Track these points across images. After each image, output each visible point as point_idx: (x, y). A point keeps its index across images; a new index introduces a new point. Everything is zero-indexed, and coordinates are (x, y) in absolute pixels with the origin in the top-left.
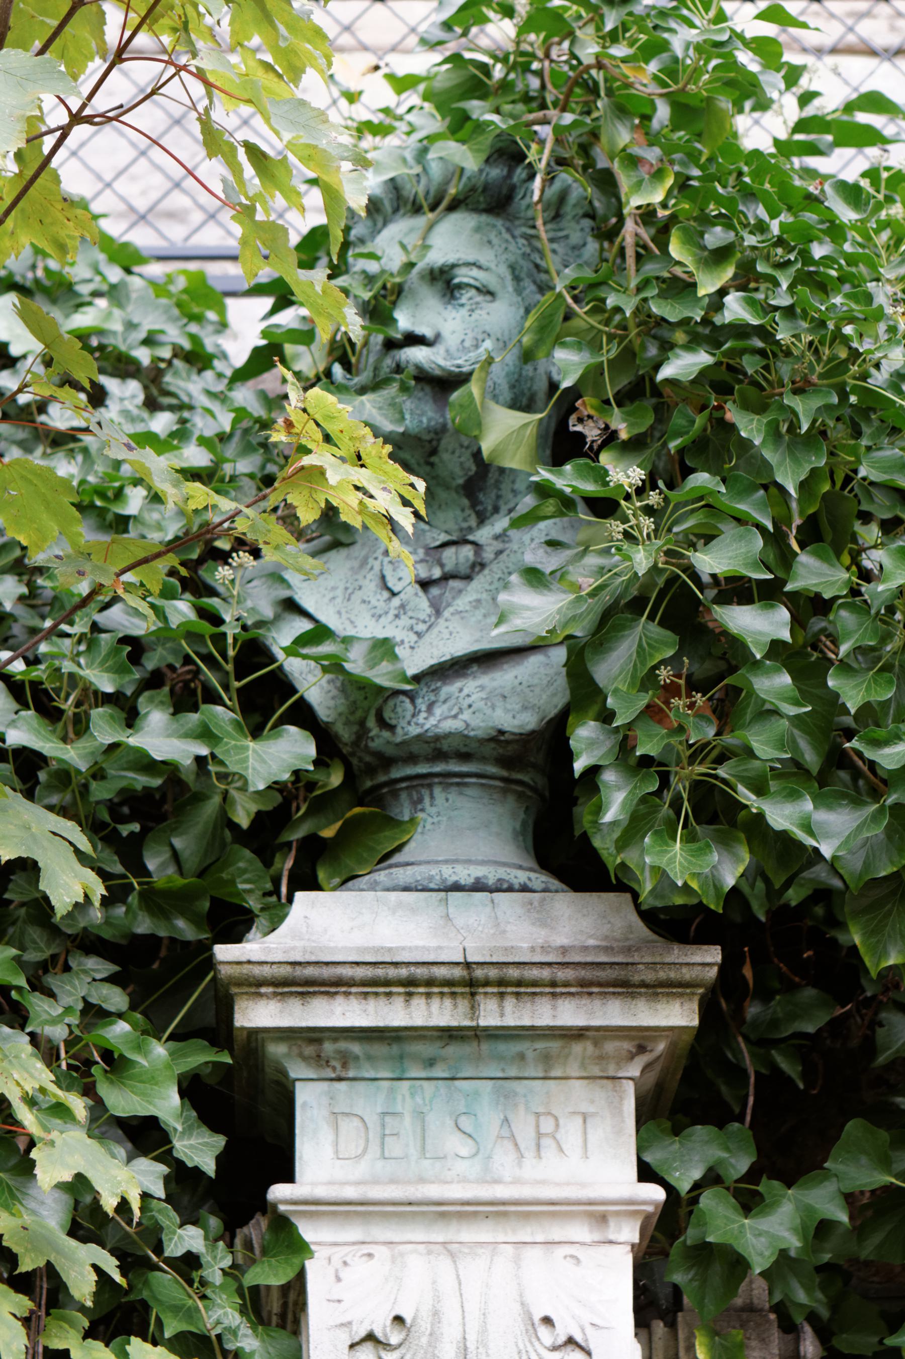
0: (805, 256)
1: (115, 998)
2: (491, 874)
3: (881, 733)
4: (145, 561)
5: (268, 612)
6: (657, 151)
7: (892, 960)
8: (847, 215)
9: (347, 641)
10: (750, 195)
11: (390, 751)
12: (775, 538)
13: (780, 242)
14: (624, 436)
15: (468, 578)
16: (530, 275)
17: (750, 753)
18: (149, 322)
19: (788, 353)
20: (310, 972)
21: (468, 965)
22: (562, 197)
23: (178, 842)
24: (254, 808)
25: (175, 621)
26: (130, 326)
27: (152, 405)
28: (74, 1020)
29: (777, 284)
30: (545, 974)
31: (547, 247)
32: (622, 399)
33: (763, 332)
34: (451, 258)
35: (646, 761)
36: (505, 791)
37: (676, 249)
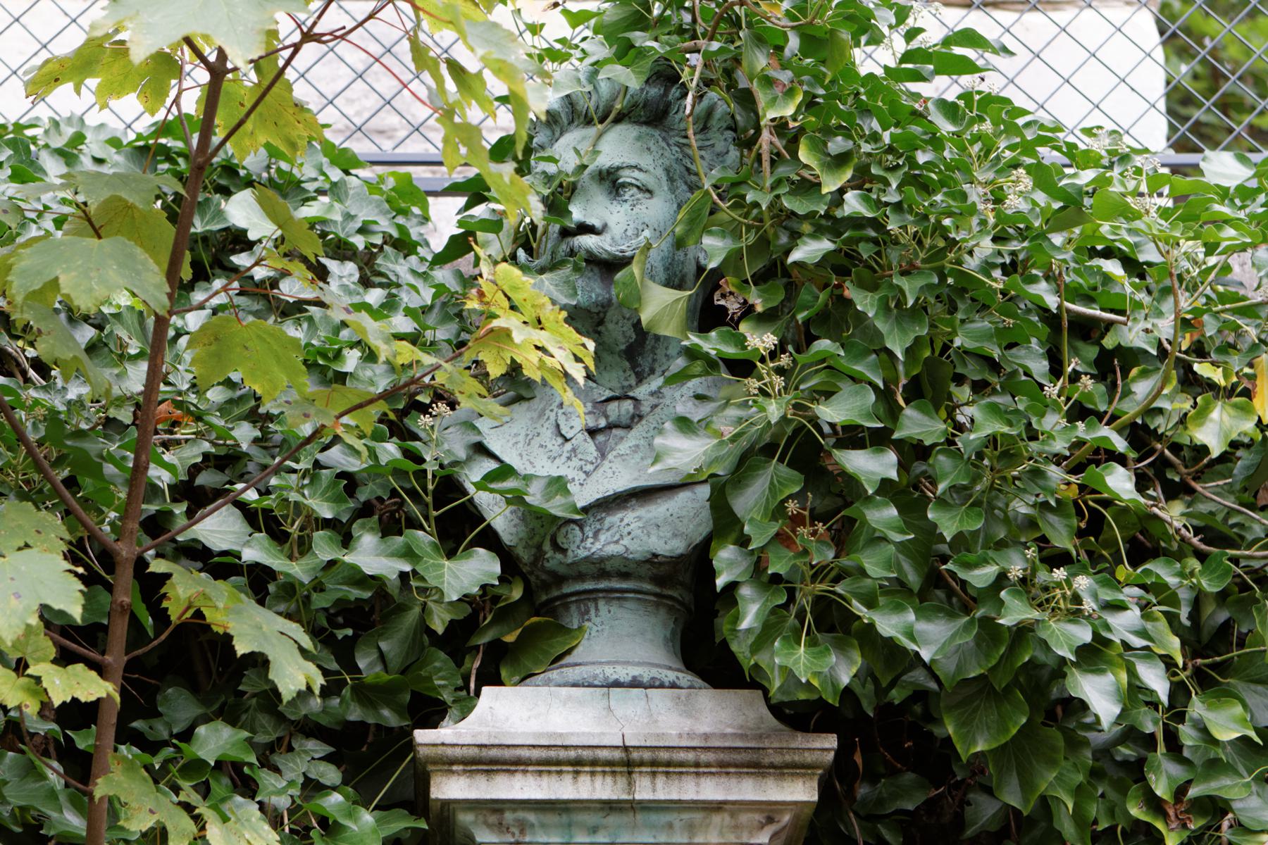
0: (912, 162)
1: (331, 775)
2: (645, 674)
3: (971, 557)
4: (360, 406)
5: (462, 454)
6: (789, 74)
7: (980, 747)
8: (946, 127)
9: (528, 478)
10: (866, 111)
11: (562, 570)
12: (885, 395)
13: (890, 150)
14: (759, 309)
15: (628, 427)
16: (682, 176)
17: (863, 573)
18: (364, 214)
19: (896, 242)
20: (494, 753)
21: (626, 748)
22: (710, 112)
23: (384, 645)
24: (448, 617)
25: (384, 460)
26: (349, 217)
27: (366, 283)
28: (296, 791)
29: (888, 184)
30: (690, 756)
31: (697, 154)
32: (759, 279)
33: (876, 224)
34: (617, 162)
35: (776, 578)
36: (657, 605)
37: (804, 155)
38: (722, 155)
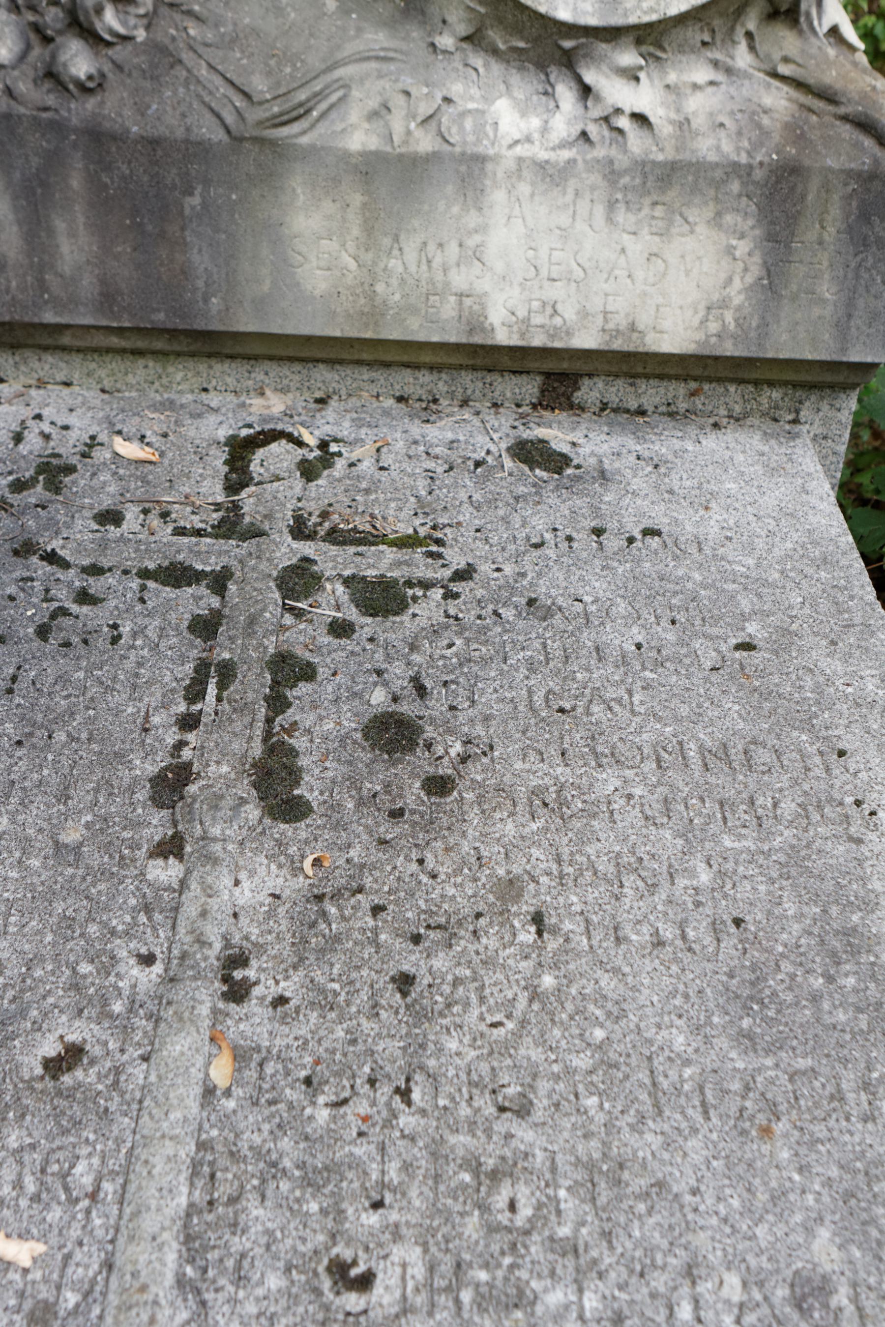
38: (505, 1098)
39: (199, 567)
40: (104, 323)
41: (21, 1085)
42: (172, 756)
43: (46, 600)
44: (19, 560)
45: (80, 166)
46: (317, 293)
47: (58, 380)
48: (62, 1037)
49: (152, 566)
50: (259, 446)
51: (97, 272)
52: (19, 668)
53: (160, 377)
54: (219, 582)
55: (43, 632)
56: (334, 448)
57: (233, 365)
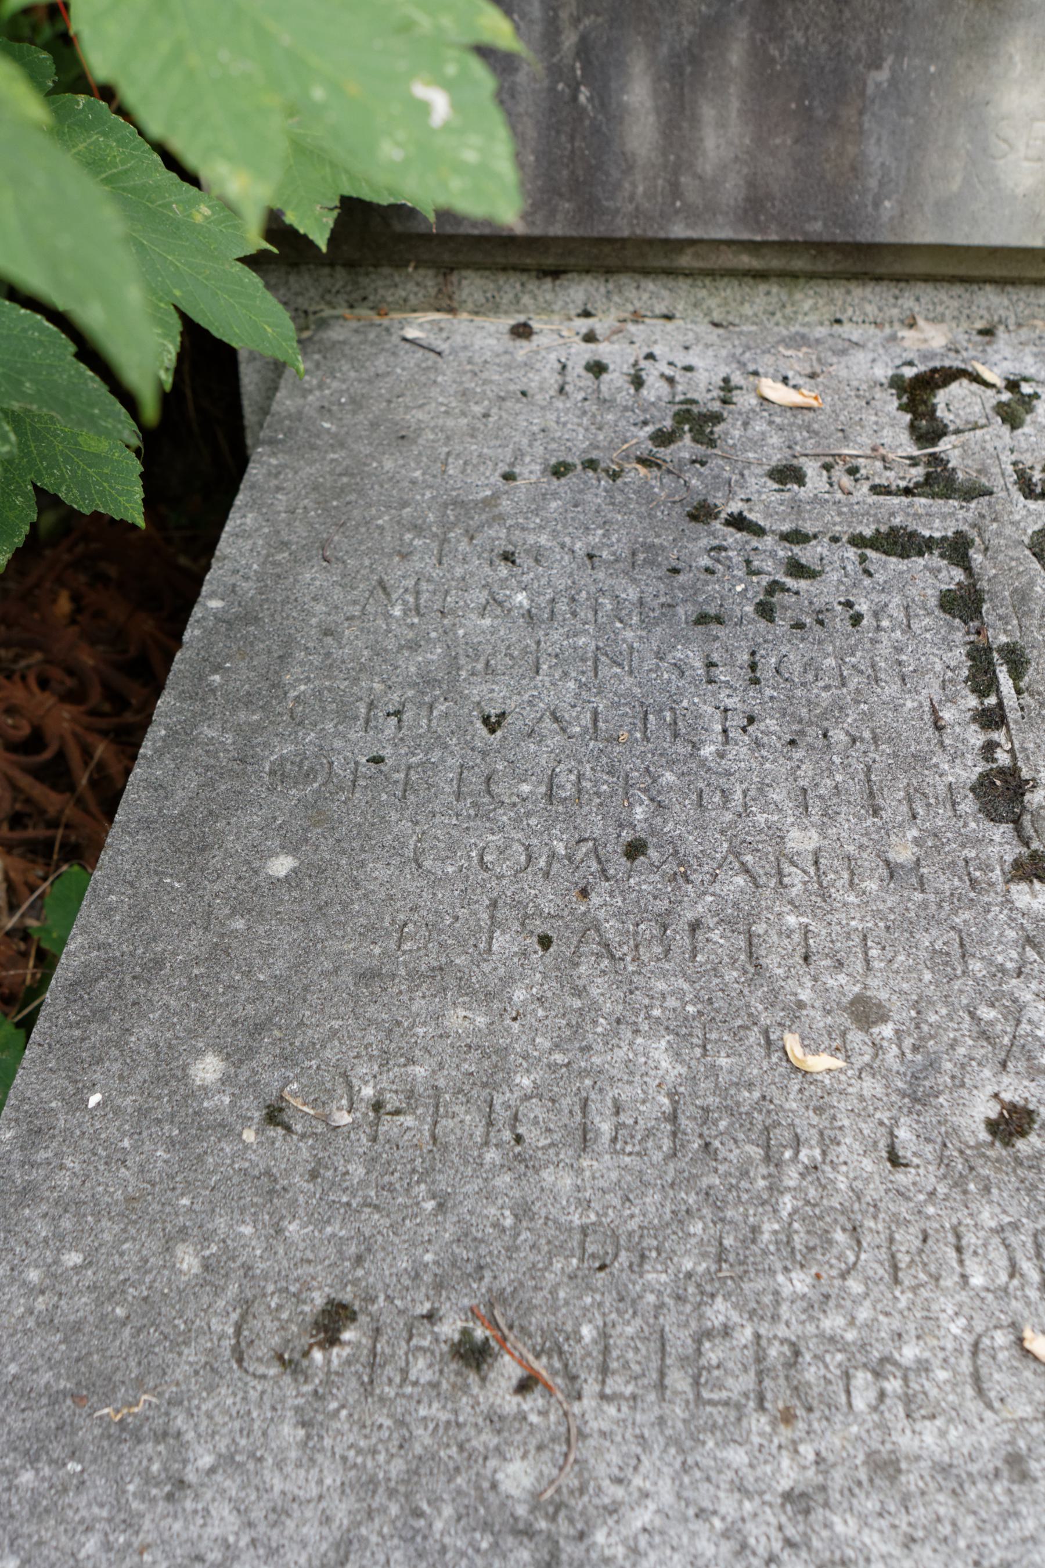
39: (927, 533)
40: (745, 236)
41: (968, 1152)
42: (987, 760)
43: (752, 573)
44: (700, 526)
45: (744, 35)
46: (1020, 191)
47: (657, 312)
48: (996, 1096)
49: (868, 532)
50: (939, 387)
51: (745, 170)
52: (753, 653)
53: (784, 306)
54: (957, 549)
55: (766, 611)
56: (1026, 389)
57: (878, 289)
